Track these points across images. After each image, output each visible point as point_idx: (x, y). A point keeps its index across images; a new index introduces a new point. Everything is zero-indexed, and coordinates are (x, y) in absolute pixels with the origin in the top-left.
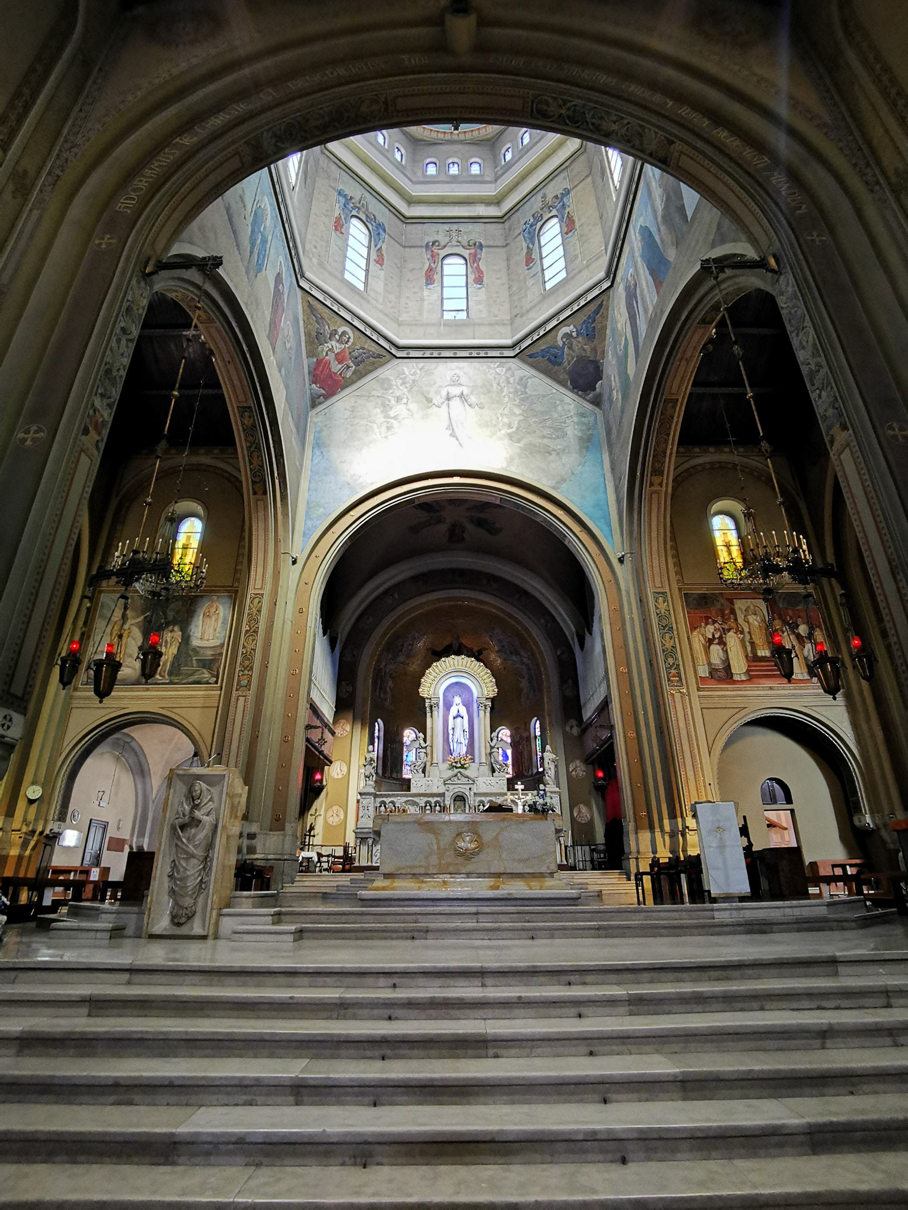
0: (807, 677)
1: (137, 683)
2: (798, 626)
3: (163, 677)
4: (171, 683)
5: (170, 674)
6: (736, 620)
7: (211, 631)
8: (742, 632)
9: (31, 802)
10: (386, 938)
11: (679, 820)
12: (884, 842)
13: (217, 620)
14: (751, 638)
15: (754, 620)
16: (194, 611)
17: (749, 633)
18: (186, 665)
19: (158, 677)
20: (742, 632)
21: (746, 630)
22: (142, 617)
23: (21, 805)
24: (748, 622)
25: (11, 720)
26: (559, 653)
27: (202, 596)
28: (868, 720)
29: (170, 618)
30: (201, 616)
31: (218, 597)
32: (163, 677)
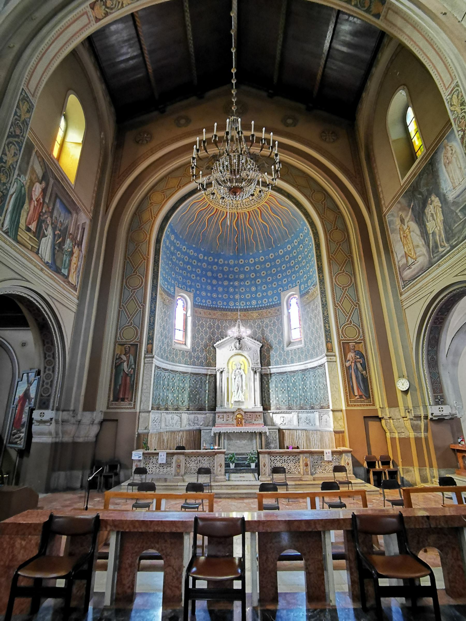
1: (431, 264)
3: (444, 246)
4: (453, 247)
5: (448, 240)
7: (458, 171)
9: (406, 392)
10: (328, 581)
13: (457, 158)
16: (437, 171)
18: (455, 222)
19: (441, 249)
22: (411, 210)
23: (400, 396)
25: (44, 413)
27: (436, 153)
29: (426, 193)
30: (443, 167)
31: (447, 138)
32: (444, 246)
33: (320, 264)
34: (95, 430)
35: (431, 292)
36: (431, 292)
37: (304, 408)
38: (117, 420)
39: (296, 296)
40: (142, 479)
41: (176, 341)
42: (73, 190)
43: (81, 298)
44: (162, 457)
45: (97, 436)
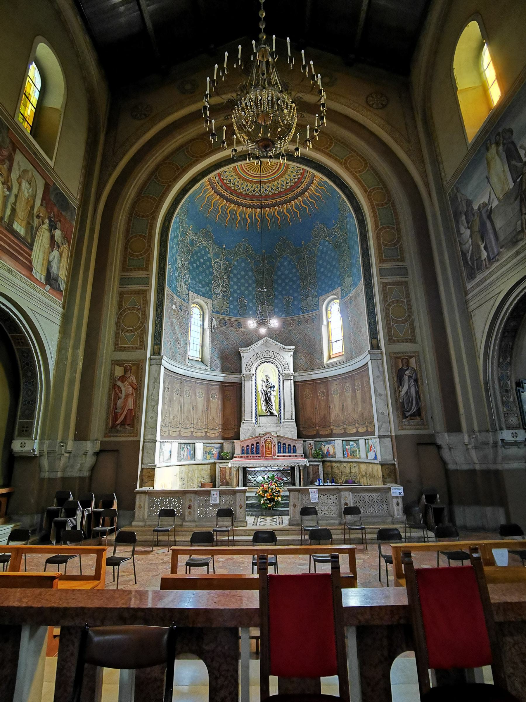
0: (43, 281)
2: (55, 229)
6: (10, 170)
8: (10, 189)
11: (298, 537)
12: (40, 468)
14: (15, 203)
15: (26, 190)
17: (16, 196)
20: (10, 189)
21: (15, 191)
24: (20, 184)
25: (21, 447)
26: (522, 313)
28: (76, 347)
33: (348, 192)
34: (90, 461)
35: (499, 293)
36: (499, 293)
37: (254, 342)
38: (117, 451)
39: (338, 301)
40: (410, 532)
41: (190, 358)
42: (53, 169)
43: (67, 306)
44: (215, 496)
45: (93, 469)
